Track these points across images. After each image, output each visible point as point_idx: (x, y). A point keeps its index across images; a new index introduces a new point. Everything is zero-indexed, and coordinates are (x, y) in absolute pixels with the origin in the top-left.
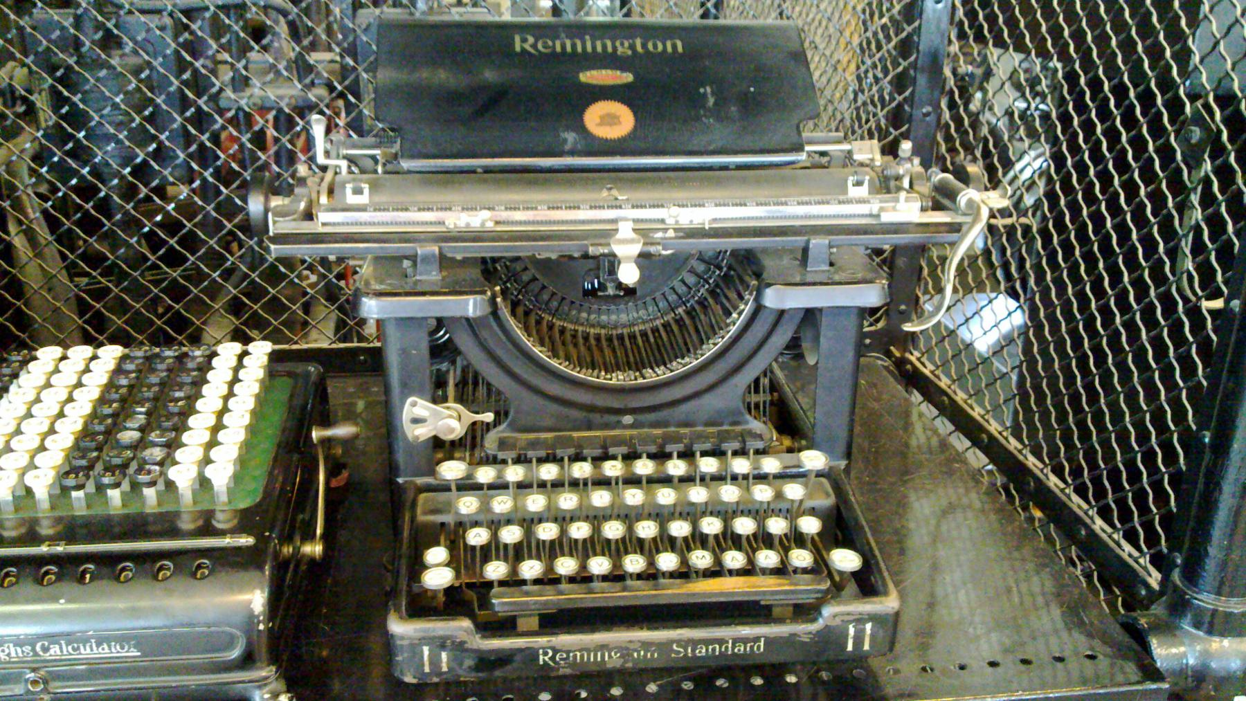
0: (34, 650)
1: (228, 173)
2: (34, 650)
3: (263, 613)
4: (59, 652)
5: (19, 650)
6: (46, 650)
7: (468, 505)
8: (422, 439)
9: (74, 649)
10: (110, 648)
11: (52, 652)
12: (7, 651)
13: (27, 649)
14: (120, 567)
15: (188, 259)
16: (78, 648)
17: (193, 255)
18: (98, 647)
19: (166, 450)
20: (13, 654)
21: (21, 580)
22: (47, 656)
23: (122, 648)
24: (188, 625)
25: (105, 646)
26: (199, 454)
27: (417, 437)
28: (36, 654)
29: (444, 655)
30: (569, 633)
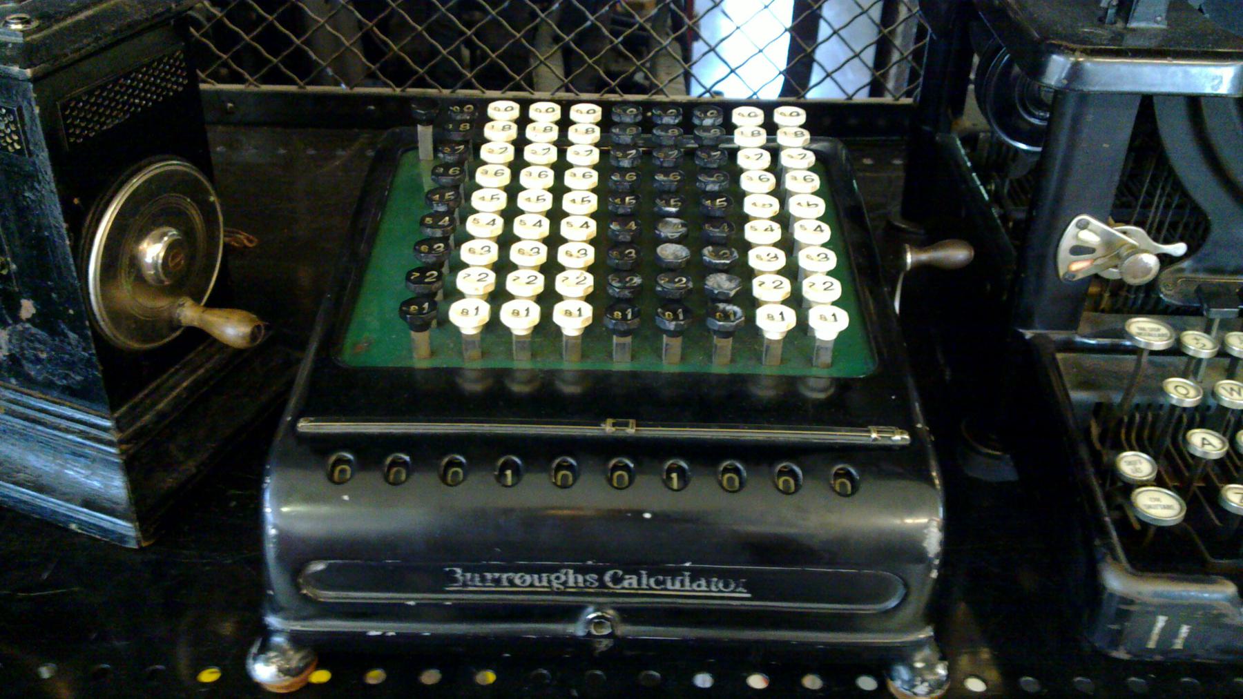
0: (601, 580)
1: (520, 59)
2: (601, 580)
3: (937, 556)
4: (635, 585)
5: (580, 578)
6: (617, 580)
7: (1182, 392)
8: (1080, 276)
9: (658, 583)
10: (708, 585)
11: (626, 584)
12: (563, 578)
13: (592, 577)
14: (333, 458)
15: (586, 19)
16: (664, 582)
17: (593, 14)
18: (692, 582)
19: (1072, 86)
20: (571, 583)
21: (639, 479)
22: (618, 589)
23: (726, 586)
24: (573, 509)
25: (703, 582)
26: (804, 260)
27: (1074, 274)
28: (603, 585)
29: (1185, 630)
30: (1172, 579)
